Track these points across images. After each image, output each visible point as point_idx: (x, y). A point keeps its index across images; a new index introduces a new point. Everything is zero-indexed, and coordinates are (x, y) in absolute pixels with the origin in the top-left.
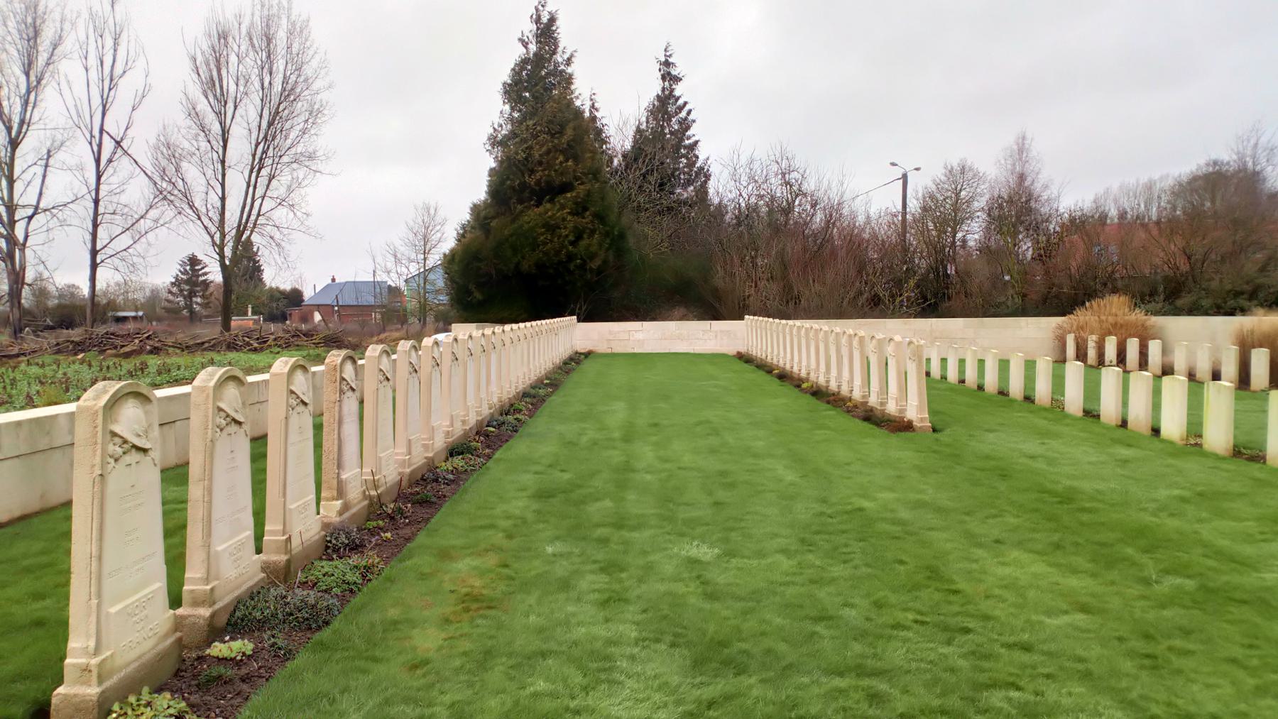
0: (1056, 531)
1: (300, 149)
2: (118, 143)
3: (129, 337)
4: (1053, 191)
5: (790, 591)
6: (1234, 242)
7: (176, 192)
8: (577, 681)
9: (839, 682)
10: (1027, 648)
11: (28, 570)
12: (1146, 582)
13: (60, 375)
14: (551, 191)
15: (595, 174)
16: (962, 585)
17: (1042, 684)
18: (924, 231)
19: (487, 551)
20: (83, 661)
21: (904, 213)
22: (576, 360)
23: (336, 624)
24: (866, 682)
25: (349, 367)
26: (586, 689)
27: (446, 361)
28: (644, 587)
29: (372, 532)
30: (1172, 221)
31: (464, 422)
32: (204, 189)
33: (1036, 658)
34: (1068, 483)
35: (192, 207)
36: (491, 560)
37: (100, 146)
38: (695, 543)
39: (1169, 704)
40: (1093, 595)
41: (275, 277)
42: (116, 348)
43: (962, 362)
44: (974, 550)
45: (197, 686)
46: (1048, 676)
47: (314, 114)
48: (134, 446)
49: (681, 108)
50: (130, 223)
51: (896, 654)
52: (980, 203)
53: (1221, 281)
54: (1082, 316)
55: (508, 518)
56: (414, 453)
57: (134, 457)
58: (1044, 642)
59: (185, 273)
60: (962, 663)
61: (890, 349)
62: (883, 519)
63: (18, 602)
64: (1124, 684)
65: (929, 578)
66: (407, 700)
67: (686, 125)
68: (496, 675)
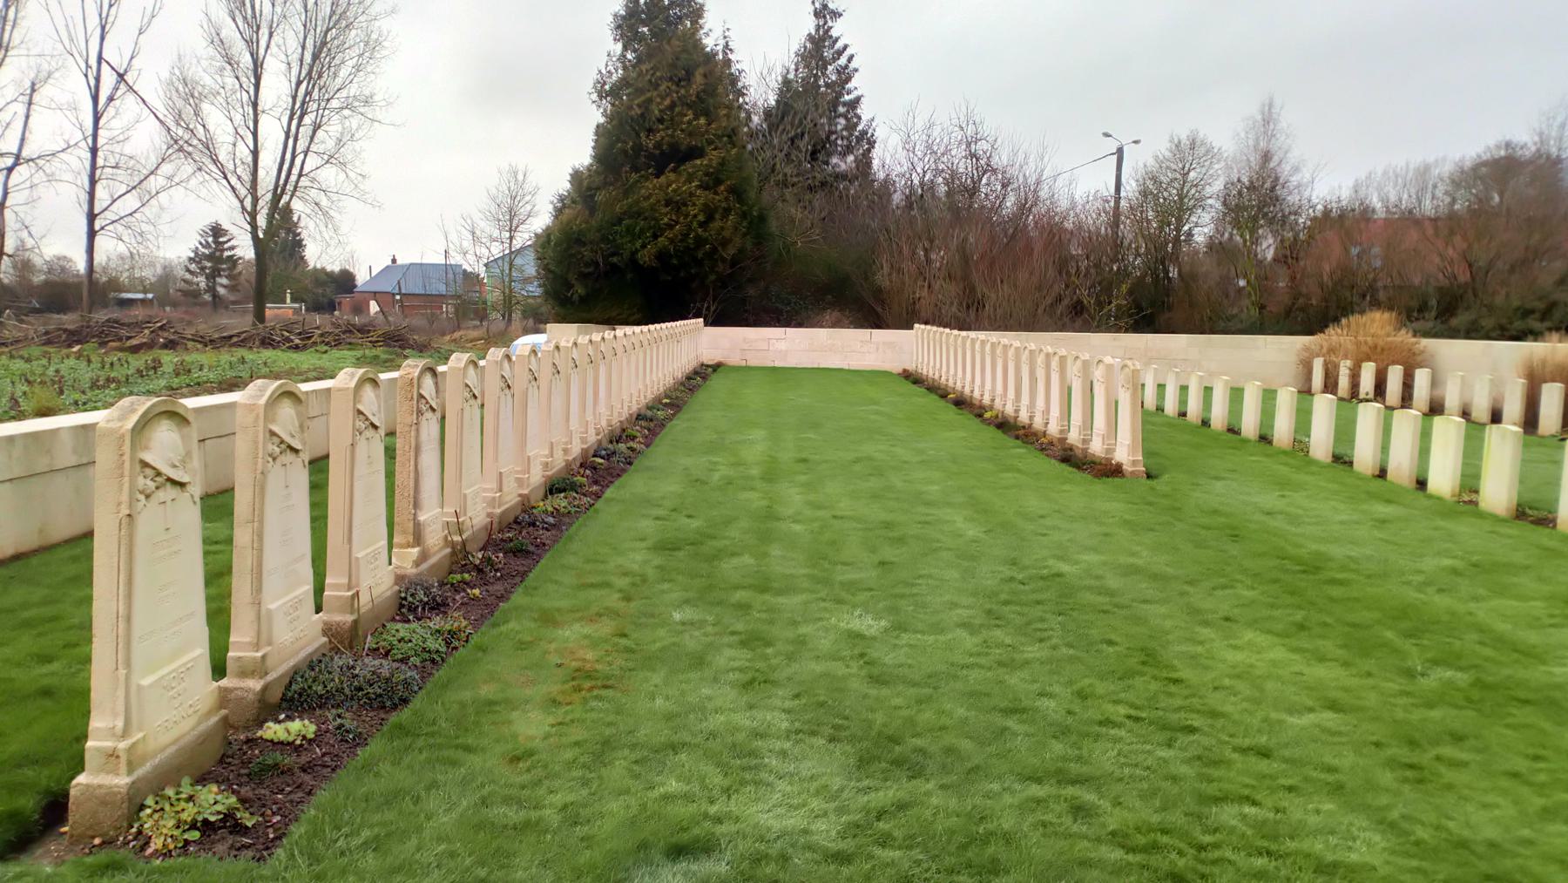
0: (1299, 607)
1: (353, 90)
2: (121, 76)
3: (138, 326)
4: (1305, 175)
5: (975, 675)
6: (1527, 248)
7: (195, 142)
8: (716, 780)
9: (1036, 790)
10: (1265, 753)
11: (27, 624)
12: (1410, 674)
13: (51, 372)
14: (674, 156)
15: (732, 135)
16: (1185, 673)
17: (1286, 801)
18: (1141, 222)
19: (600, 615)
20: (109, 744)
21: (1118, 199)
22: (702, 374)
23: (417, 703)
24: (1070, 791)
25: (428, 381)
26: (727, 791)
27: (545, 373)
28: (795, 667)
29: (456, 588)
30: (1452, 216)
31: (566, 451)
32: (231, 139)
33: (1276, 766)
34: (1314, 547)
35: (215, 161)
36: (606, 628)
37: (98, 79)
38: (857, 613)
39: (1438, 828)
40: (1346, 690)
41: (319, 254)
42: (120, 339)
43: (1184, 389)
44: (1198, 629)
45: (248, 775)
46: (1290, 789)
47: (371, 47)
48: (169, 480)
49: (840, 53)
50: (137, 180)
51: (1104, 756)
52: (1218, 186)
53: (1507, 295)
54: (1334, 335)
55: (625, 574)
56: (505, 489)
57: (170, 492)
58: (1287, 745)
59: (207, 246)
60: (1184, 770)
61: (1098, 374)
62: (1089, 588)
63: (19, 665)
64: (1384, 800)
65: (1144, 663)
66: (507, 800)
67: (845, 75)
68: (617, 770)
